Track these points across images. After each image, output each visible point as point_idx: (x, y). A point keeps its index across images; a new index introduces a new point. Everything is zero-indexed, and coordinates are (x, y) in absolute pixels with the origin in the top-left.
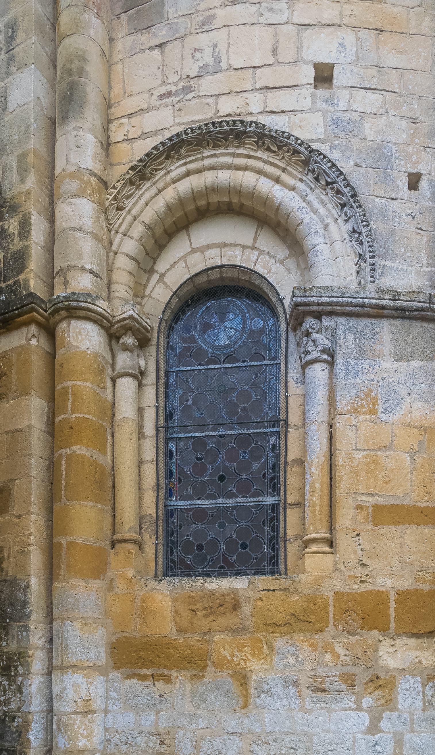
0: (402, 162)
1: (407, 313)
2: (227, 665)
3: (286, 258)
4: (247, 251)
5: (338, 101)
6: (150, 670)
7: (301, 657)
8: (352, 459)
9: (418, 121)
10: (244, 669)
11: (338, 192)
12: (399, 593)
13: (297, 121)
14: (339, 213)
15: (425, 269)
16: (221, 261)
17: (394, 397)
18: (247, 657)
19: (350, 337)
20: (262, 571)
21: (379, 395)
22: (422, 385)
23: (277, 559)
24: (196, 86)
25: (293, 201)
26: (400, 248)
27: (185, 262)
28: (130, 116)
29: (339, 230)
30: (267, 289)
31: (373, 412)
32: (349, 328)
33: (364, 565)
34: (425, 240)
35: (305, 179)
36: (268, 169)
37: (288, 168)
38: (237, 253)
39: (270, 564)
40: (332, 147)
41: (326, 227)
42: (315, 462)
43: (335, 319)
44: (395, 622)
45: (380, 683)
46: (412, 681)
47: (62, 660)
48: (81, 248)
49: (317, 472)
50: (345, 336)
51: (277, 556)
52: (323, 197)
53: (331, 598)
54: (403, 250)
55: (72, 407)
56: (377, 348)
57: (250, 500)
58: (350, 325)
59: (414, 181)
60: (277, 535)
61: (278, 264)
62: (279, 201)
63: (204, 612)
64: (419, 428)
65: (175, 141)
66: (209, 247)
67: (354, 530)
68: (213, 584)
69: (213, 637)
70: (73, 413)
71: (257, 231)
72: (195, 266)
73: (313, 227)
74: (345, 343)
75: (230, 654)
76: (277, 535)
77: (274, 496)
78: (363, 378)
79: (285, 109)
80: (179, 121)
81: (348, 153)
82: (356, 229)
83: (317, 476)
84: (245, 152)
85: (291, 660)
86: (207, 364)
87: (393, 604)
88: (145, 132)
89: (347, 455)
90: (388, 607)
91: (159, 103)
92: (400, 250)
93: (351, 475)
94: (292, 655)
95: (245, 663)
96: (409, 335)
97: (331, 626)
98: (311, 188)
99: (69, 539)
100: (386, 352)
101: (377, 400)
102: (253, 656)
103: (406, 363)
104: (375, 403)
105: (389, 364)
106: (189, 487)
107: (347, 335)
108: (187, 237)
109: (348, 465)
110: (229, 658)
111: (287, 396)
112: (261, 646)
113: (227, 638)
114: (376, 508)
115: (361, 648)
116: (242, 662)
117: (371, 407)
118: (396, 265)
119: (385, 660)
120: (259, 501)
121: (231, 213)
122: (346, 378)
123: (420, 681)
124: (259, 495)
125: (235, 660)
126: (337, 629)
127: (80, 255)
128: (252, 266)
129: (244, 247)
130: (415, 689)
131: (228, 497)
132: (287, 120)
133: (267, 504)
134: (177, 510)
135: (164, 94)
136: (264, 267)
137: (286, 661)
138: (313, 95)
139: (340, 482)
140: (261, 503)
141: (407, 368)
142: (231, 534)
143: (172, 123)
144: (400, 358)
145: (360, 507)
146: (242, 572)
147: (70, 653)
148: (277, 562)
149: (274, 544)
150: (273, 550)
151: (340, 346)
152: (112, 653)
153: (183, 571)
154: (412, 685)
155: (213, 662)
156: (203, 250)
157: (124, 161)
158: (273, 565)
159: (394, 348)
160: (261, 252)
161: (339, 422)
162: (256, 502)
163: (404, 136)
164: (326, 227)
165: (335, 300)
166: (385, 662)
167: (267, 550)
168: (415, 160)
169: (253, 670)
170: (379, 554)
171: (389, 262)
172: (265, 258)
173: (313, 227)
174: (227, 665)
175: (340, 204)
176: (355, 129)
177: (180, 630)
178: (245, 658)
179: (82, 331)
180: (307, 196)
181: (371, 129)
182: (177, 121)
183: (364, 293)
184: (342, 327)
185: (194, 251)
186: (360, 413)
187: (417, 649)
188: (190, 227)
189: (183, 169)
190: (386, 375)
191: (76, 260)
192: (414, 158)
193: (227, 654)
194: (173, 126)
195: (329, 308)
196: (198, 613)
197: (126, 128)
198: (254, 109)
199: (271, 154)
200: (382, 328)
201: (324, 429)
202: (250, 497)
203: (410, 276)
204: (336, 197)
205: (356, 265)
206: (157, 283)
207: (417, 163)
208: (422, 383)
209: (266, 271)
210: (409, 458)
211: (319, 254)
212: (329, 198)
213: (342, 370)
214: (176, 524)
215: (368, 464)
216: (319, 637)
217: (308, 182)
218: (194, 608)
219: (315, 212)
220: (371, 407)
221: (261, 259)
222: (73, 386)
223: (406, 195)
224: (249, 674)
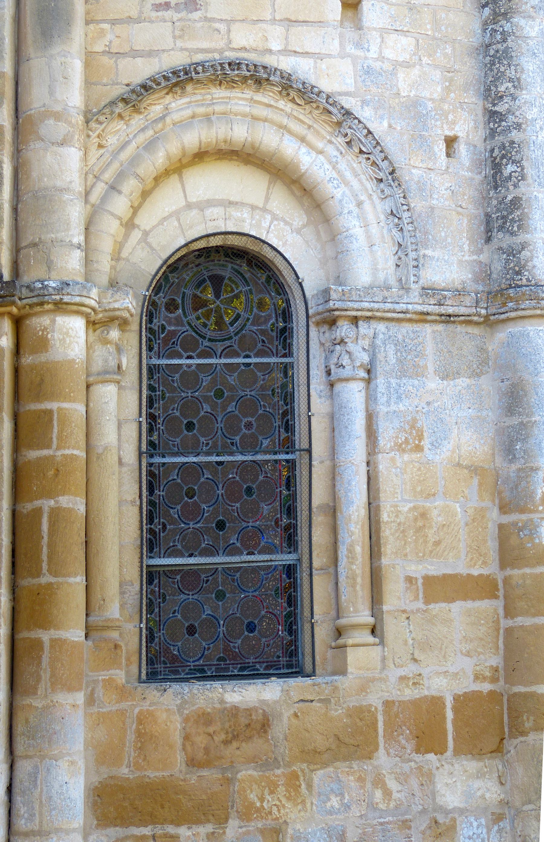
0: (438, 123)
1: (452, 319)
2: (255, 816)
3: (304, 226)
4: (257, 215)
5: (369, 46)
6: (150, 828)
7: (347, 797)
8: (398, 513)
9: (453, 70)
10: (277, 819)
11: (374, 164)
12: (456, 698)
13: (324, 67)
14: (374, 188)
15: (467, 258)
16: (225, 225)
17: (440, 428)
18: (280, 801)
19: (391, 350)
20: (275, 666)
21: (425, 425)
22: (470, 410)
23: (295, 646)
24: (202, 4)
25: (322, 170)
26: (440, 231)
27: (179, 220)
28: (114, 22)
29: (376, 209)
30: (269, 254)
31: (419, 448)
32: (390, 337)
33: (415, 660)
34: (466, 221)
35: (335, 141)
36: (294, 126)
37: (315, 126)
38: (245, 215)
39: (286, 653)
40: (364, 103)
41: (359, 204)
42: (354, 517)
43: (374, 324)
44: (454, 740)
45: (440, 831)
46: (475, 824)
47: (41, 822)
48: (68, 215)
49: (357, 531)
50: (385, 348)
51: (295, 641)
52: (355, 165)
53: (380, 708)
54: (443, 234)
55: (58, 439)
56: (421, 363)
57: (259, 558)
58: (391, 333)
59: (450, 142)
60: (295, 610)
61: (295, 234)
62: (305, 168)
63: (223, 736)
64: (467, 467)
65: (181, 79)
66: (210, 203)
67: (404, 611)
68: (235, 694)
69: (237, 773)
70: (58, 449)
71: (268, 188)
72: (191, 227)
73: (346, 205)
74: (385, 357)
75: (259, 799)
76: (295, 610)
77: (290, 553)
78: (407, 404)
79: (310, 51)
80: (182, 44)
81: (380, 112)
82: (395, 212)
83: (357, 536)
84: (265, 100)
85: (335, 802)
86: (199, 356)
87: (450, 715)
88: (135, 48)
89: (393, 509)
90: (444, 718)
91: (154, 14)
92: (441, 236)
93: (397, 535)
94: (336, 796)
95: (279, 811)
96: (453, 345)
97: (382, 750)
98: (341, 153)
99: (53, 633)
100: (431, 368)
101: (422, 432)
102: (289, 799)
103: (452, 382)
104: (421, 437)
105: (433, 384)
106: (177, 537)
107: (388, 347)
108: (179, 186)
109: (394, 521)
110: (258, 804)
111: (309, 417)
112: (298, 783)
113: (255, 773)
114: (428, 580)
115: (417, 780)
116: (275, 809)
117: (417, 442)
118: (436, 254)
119: (444, 795)
120: (271, 561)
121: (236, 160)
122: (388, 402)
123: (484, 823)
124: (271, 552)
125: (266, 807)
126: (388, 754)
127: (68, 224)
128: (264, 235)
129: (254, 208)
130: (478, 836)
131: (231, 554)
132: (312, 65)
133: (281, 565)
134: (159, 573)
135: (160, 4)
136: (278, 238)
137: (329, 804)
138: (341, 36)
139: (385, 545)
140: (273, 563)
141: (453, 389)
142: (234, 610)
143: (172, 45)
144: (445, 376)
145: (410, 580)
146: (248, 667)
147: (54, 809)
148: (295, 650)
149: (291, 623)
150: (290, 634)
151: (381, 361)
152: (95, 804)
153: (168, 665)
154: (475, 831)
155: (237, 812)
156: (202, 206)
157: (105, 81)
158: (291, 656)
159: (438, 363)
160: (275, 217)
161: (383, 463)
162: (267, 561)
163: (439, 89)
164: (359, 204)
165: (376, 306)
166: (444, 799)
167: (282, 633)
168: (452, 119)
169: (288, 821)
170: (432, 645)
171: (430, 251)
172: (279, 224)
173: (346, 205)
174: (255, 816)
175: (376, 178)
176: (388, 82)
177: (192, 763)
178: (278, 803)
179: (70, 331)
180: (337, 163)
181: (405, 81)
182: (179, 44)
183: (408, 297)
184: (381, 336)
185: (189, 206)
186: (404, 451)
187: (478, 777)
188: (184, 171)
189: (188, 112)
190: (431, 399)
191: (62, 231)
192: (451, 117)
193: (256, 799)
194: (173, 49)
195: (369, 314)
196: (215, 737)
197: (109, 36)
198: (275, 46)
199: (295, 107)
200: (425, 336)
201: (363, 469)
202: (260, 553)
203: (452, 268)
204: (372, 169)
205: (394, 255)
206: (139, 243)
207: (454, 123)
208: (469, 408)
209: (281, 243)
210: (459, 510)
211: (354, 241)
212: (361, 165)
213: (383, 394)
214: (157, 594)
215: (416, 519)
216: (367, 766)
217: (338, 145)
218: (211, 730)
219: (347, 183)
220: (417, 442)
221: (275, 225)
222: (60, 409)
223: (444, 164)
224: (284, 827)
